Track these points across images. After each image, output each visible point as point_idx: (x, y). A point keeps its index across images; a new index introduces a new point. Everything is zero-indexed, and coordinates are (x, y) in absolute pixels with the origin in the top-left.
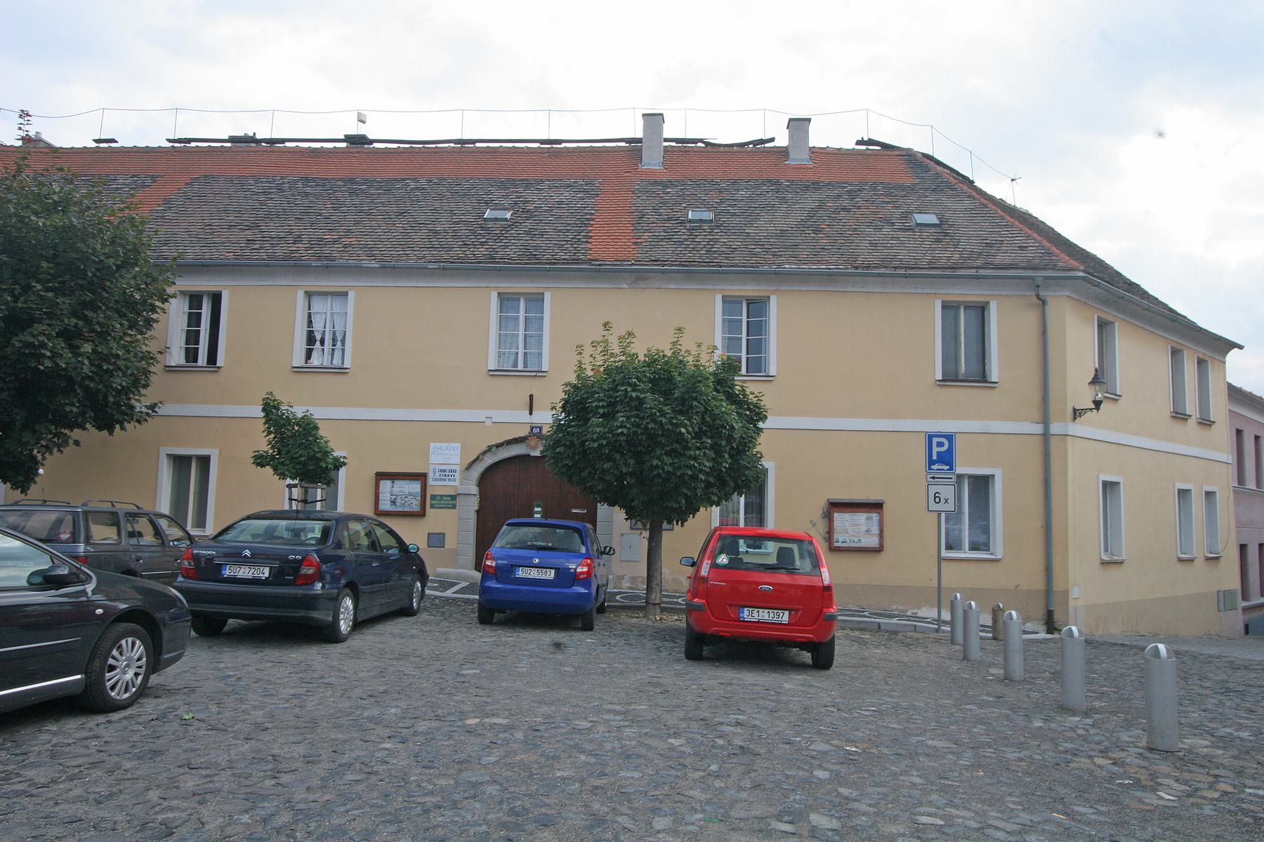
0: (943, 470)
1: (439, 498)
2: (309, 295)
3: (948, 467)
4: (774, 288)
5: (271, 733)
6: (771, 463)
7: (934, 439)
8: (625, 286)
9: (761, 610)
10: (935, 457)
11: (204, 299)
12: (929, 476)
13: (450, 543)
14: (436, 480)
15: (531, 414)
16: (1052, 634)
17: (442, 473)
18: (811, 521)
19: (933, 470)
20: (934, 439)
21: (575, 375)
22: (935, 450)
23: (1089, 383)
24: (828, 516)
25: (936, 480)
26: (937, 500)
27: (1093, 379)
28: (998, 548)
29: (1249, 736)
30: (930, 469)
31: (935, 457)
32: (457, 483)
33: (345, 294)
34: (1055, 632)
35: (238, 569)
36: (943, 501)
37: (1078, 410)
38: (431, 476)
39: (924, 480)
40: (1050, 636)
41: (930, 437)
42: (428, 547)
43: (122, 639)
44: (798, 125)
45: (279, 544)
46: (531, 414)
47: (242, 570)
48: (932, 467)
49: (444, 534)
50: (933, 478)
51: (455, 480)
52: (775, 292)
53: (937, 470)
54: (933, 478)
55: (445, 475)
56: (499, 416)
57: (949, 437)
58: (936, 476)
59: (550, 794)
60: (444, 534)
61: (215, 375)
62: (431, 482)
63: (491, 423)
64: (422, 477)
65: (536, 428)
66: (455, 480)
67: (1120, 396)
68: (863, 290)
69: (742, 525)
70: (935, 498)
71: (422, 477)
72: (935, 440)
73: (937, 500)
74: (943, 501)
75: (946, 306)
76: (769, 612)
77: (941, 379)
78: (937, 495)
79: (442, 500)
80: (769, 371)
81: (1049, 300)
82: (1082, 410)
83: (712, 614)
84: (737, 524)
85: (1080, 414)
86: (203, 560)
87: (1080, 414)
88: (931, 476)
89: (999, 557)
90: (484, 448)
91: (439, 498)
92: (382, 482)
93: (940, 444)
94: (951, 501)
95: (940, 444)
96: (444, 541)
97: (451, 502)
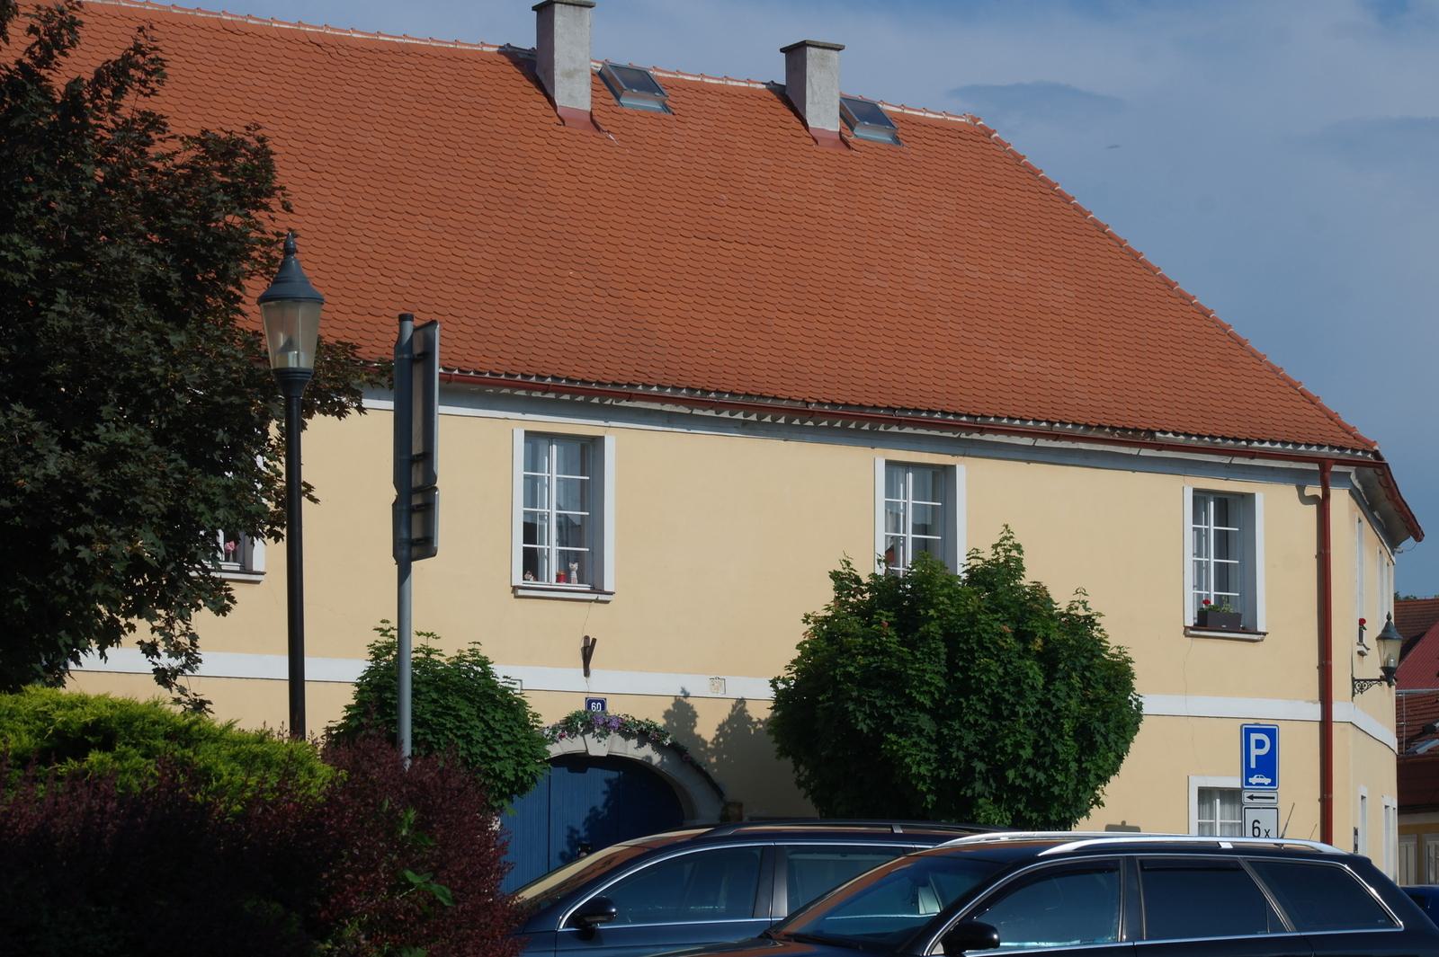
0: (1263, 784)
3: (1269, 781)
6: (588, 99)
7: (1252, 735)
10: (1253, 765)
15: (587, 673)
19: (1251, 784)
20: (1252, 735)
21: (239, 132)
22: (1254, 752)
26: (1256, 831)
31: (1253, 765)
36: (1263, 834)
37: (1359, 681)
45: (915, 849)
46: (587, 673)
48: (1251, 780)
53: (1257, 784)
58: (1255, 795)
65: (596, 701)
70: (1254, 828)
72: (1254, 737)
73: (1256, 831)
74: (1263, 834)
78: (1256, 824)
82: (1365, 681)
85: (1362, 688)
86: (986, 807)
87: (1362, 688)
88: (1249, 794)
93: (1260, 744)
95: (1260, 744)
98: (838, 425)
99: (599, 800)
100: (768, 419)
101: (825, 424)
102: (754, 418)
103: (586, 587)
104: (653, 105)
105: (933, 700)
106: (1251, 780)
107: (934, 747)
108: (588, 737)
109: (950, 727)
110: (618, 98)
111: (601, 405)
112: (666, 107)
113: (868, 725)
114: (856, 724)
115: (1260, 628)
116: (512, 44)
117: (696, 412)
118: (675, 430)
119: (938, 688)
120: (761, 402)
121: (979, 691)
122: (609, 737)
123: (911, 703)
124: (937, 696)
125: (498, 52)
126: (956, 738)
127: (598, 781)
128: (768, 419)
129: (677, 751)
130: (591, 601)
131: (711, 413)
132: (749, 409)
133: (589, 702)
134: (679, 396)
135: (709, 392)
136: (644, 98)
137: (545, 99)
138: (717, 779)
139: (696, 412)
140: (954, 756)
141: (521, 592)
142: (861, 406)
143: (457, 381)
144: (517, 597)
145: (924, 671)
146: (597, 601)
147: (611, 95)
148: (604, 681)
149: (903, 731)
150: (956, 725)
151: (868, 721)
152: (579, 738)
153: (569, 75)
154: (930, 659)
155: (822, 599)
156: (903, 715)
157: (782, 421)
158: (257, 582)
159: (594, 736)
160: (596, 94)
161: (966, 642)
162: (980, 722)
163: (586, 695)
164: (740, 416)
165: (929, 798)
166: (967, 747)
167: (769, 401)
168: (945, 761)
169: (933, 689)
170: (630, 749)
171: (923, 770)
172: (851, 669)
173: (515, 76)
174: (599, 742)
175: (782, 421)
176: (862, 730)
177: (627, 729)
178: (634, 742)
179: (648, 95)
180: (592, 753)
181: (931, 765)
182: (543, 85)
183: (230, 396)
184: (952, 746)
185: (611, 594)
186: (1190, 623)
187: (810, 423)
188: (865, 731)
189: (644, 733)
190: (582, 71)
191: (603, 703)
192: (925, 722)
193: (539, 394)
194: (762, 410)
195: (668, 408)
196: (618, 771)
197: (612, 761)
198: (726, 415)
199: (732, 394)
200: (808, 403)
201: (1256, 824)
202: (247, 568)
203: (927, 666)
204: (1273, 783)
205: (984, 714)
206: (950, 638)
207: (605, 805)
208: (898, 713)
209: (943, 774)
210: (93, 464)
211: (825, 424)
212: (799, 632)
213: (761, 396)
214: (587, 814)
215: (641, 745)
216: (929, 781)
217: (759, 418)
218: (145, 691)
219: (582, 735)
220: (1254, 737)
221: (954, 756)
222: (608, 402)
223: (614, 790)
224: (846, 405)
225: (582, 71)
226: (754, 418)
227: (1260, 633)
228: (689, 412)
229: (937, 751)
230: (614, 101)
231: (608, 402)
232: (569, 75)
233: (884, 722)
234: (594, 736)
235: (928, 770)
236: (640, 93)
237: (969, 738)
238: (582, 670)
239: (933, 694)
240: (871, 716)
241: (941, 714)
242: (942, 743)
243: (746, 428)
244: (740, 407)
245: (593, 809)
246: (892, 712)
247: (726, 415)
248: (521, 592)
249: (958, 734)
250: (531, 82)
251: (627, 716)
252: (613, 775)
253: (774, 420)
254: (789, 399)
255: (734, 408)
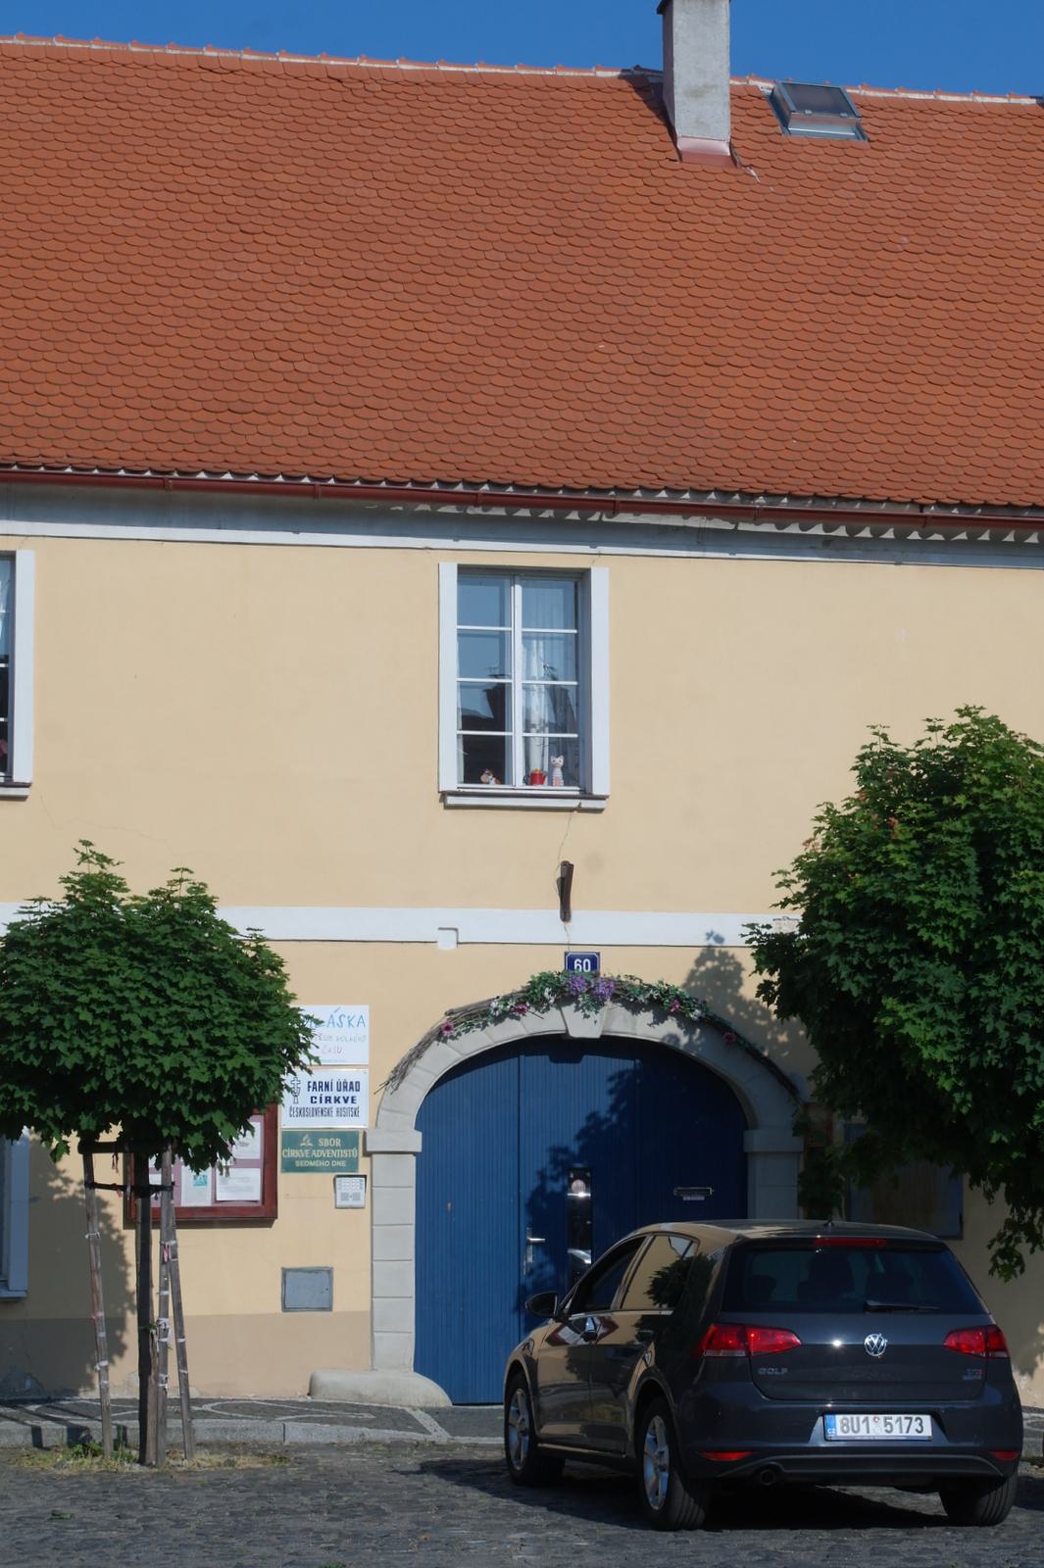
1: (307, 1142)
9: (871, 1417)
11: (447, 1398)
13: (349, 1295)
14: (302, 1112)
15: (566, 915)
17: (317, 1094)
35: (906, 1423)
42: (285, 1309)
46: (566, 915)
47: (915, 1425)
49: (329, 1271)
51: (355, 1113)
55: (328, 1099)
56: (479, 923)
60: (329, 1271)
63: (453, 946)
65: (582, 958)
66: (355, 1113)
69: (708, 1353)
76: (900, 1419)
79: (316, 1147)
84: (710, 1346)
90: (438, 1018)
91: (307, 1142)
96: (330, 1289)
97: (345, 1153)
98: (986, 537)
99: (602, 1102)
100: (866, 533)
101: (963, 536)
102: (842, 532)
103: (574, 790)
104: (840, 130)
105: (957, 942)
107: (954, 1017)
108: (569, 1010)
109: (979, 983)
110: (785, 123)
111: (583, 524)
112: (861, 133)
113: (858, 983)
114: (841, 982)
115: (18, 776)
117: (742, 527)
118: (708, 554)
119: (966, 923)
120: (844, 507)
121: (1020, 923)
122: (603, 1010)
123: (926, 950)
124: (962, 935)
125: (620, 77)
126: (990, 1000)
127: (600, 1074)
128: (866, 533)
129: (713, 1024)
130: (571, 810)
131: (768, 528)
132: (831, 519)
133: (570, 961)
134: (705, 503)
135: (754, 496)
136: (830, 123)
137: (665, 129)
138: (786, 1069)
139: (742, 527)
140: (989, 1029)
141: (451, 800)
142: (1010, 506)
143: (177, 487)
144: (448, 807)
145: (936, 894)
146: (580, 809)
147: (777, 121)
148: (590, 928)
149: (908, 993)
150: (990, 979)
151: (858, 977)
152: (554, 1011)
153: (696, 93)
154: (948, 874)
155: (843, 788)
156: (910, 966)
157: (889, 535)
158: (23, 798)
159: (577, 1009)
160: (738, 119)
161: (1006, 845)
162: (1027, 972)
163: (565, 949)
164: (818, 530)
165: (958, 1097)
166: (1010, 1013)
167: (858, 506)
168: (978, 1040)
169: (954, 923)
170: (643, 1027)
171: (940, 1054)
172: (841, 896)
173: (634, 105)
174: (587, 1016)
175: (889, 535)
176: (849, 992)
177: (628, 996)
178: (647, 1016)
179: (831, 116)
180: (575, 1033)
181: (954, 1044)
182: (663, 110)
184: (985, 1013)
185: (602, 798)
187: (937, 537)
188: (855, 993)
189: (660, 1002)
190: (715, 86)
191: (594, 961)
192: (949, 981)
193: (479, 511)
194: (855, 520)
195: (695, 522)
196: (634, 1059)
197: (609, 1045)
198: (794, 529)
199: (791, 496)
200: (922, 507)
202: (588, 791)
203: (942, 889)
205: (1032, 961)
206: (984, 841)
207: (613, 1109)
208: (900, 965)
209: (973, 1061)
211: (963, 536)
213: (840, 498)
214: (583, 1124)
215: (660, 1019)
216: (953, 1071)
217: (852, 532)
219: (559, 1008)
221: (989, 1029)
222: (595, 518)
223: (624, 1088)
224: (986, 505)
225: (715, 86)
226: (842, 532)
228: (732, 527)
229: (964, 1023)
230: (779, 129)
231: (595, 518)
232: (696, 93)
233: (882, 981)
234: (577, 1009)
235: (951, 1054)
236: (817, 115)
237: (1012, 998)
238: (557, 912)
239: (957, 931)
240: (859, 969)
241: (972, 960)
242: (971, 1010)
243: (828, 547)
244: (982, 523)
245: (593, 1116)
246: (891, 963)
247: (818, 530)
248: (451, 800)
249: (992, 993)
250: (651, 108)
251: (631, 977)
252: (628, 1065)
253: (877, 534)
254: (888, 500)
255: (807, 517)
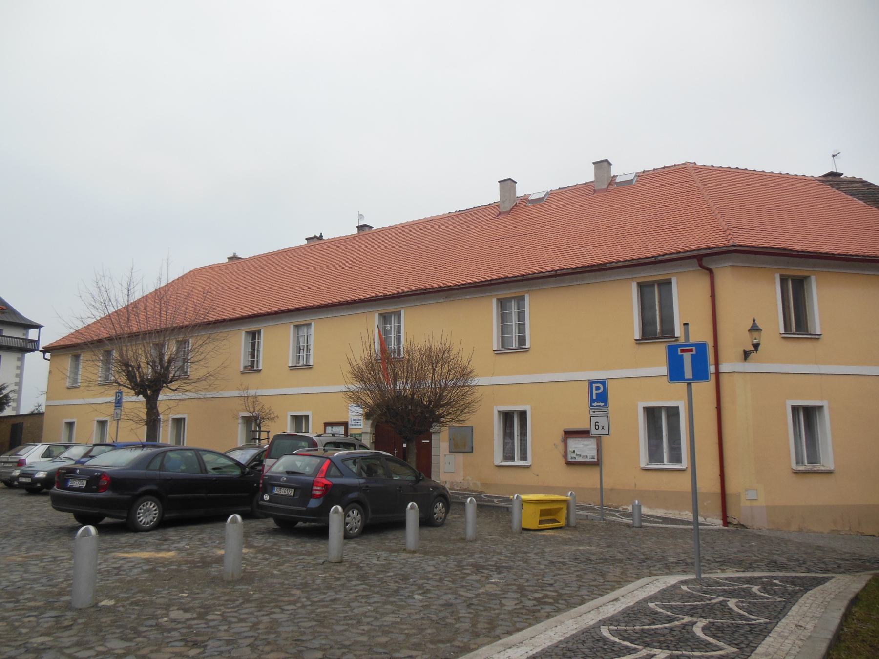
2: (297, 327)
3: (602, 404)
4: (527, 289)
5: (345, 565)
8: (442, 300)
10: (594, 397)
12: (591, 411)
14: (352, 425)
16: (727, 526)
18: (554, 445)
22: (595, 392)
23: (749, 331)
24: (565, 442)
25: (596, 413)
26: (597, 427)
27: (752, 327)
28: (827, 461)
29: (516, 605)
30: (592, 406)
31: (594, 397)
32: (362, 427)
33: (310, 324)
34: (729, 525)
36: (601, 428)
38: (350, 423)
39: (610, 411)
40: (726, 528)
41: (591, 383)
43: (349, 511)
44: (603, 165)
48: (593, 404)
50: (594, 412)
52: (528, 292)
54: (594, 412)
57: (603, 382)
59: (793, 626)
61: (258, 374)
62: (350, 427)
64: (345, 424)
67: (820, 335)
68: (582, 282)
70: (595, 425)
71: (345, 424)
72: (594, 385)
73: (597, 427)
74: (601, 428)
75: (641, 286)
77: (784, 332)
78: (597, 424)
80: (809, 330)
81: (715, 271)
83: (277, 503)
89: (831, 467)
92: (327, 427)
93: (598, 388)
94: (606, 427)
95: (598, 388)
106: (593, 404)
116: (244, 254)
183: (699, 638)
186: (637, 336)
201: (597, 424)
204: (605, 405)
210: (426, 399)
212: (48, 344)
218: (13, 413)
220: (594, 385)
227: (818, 335)
